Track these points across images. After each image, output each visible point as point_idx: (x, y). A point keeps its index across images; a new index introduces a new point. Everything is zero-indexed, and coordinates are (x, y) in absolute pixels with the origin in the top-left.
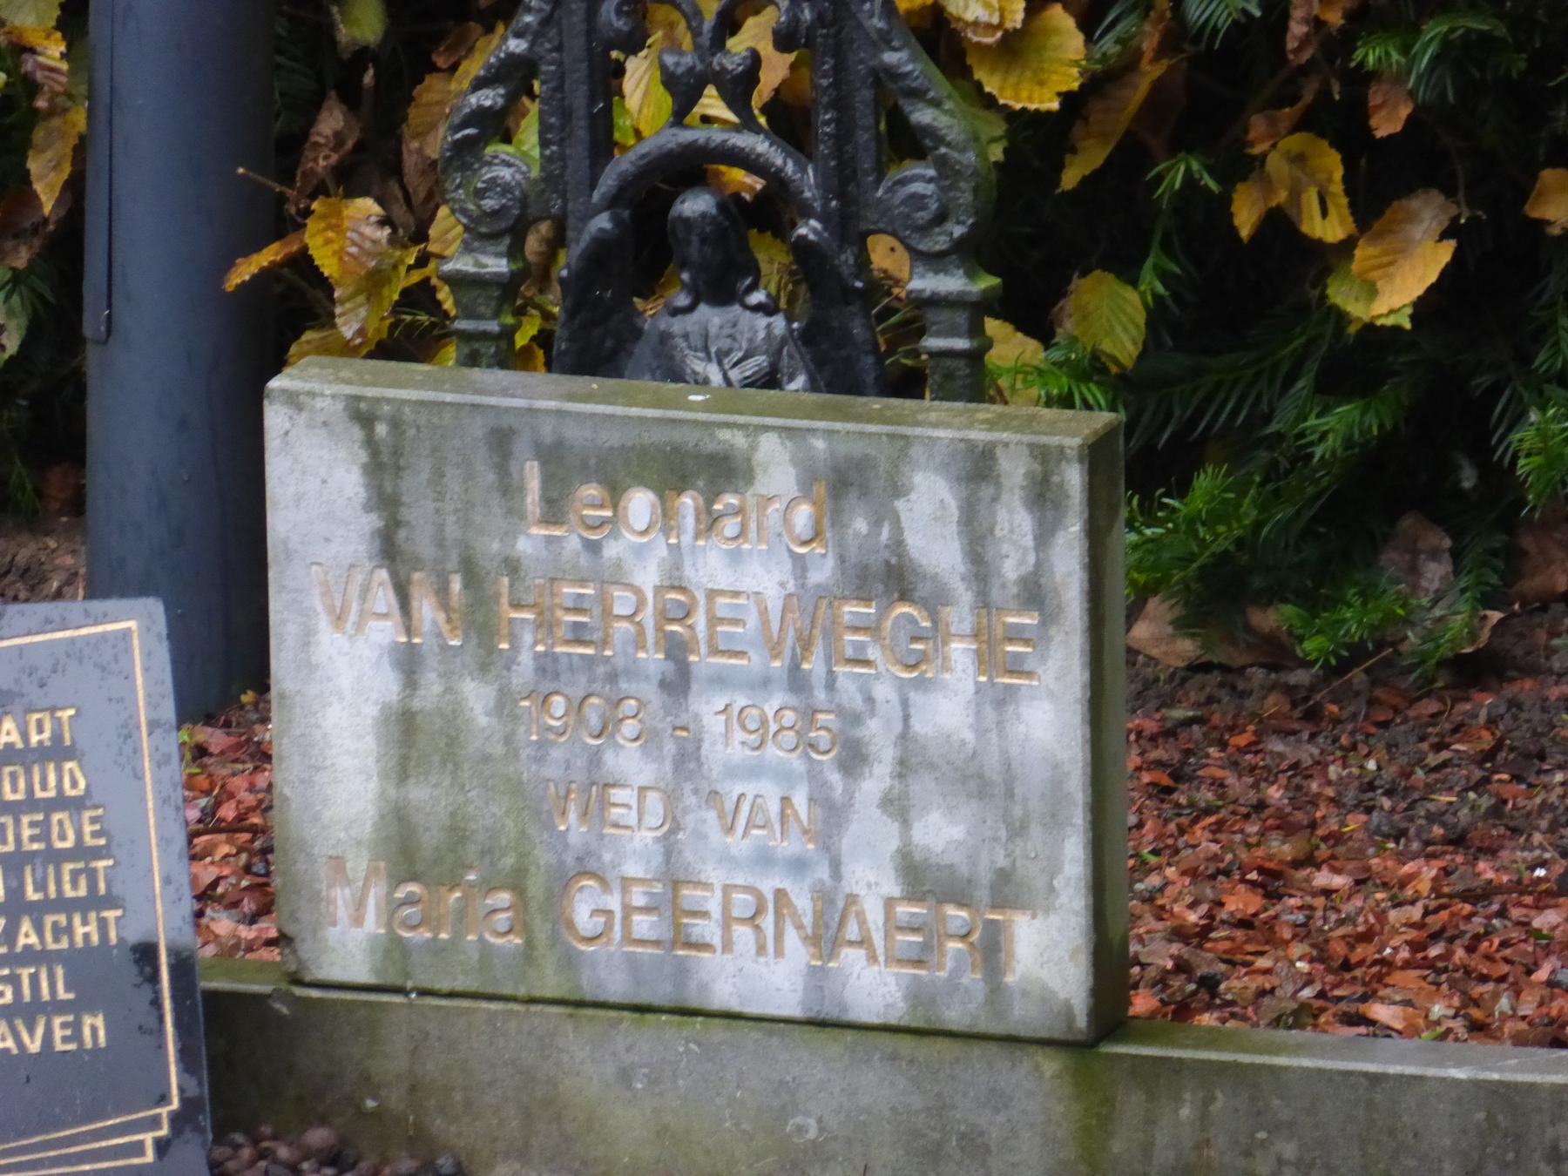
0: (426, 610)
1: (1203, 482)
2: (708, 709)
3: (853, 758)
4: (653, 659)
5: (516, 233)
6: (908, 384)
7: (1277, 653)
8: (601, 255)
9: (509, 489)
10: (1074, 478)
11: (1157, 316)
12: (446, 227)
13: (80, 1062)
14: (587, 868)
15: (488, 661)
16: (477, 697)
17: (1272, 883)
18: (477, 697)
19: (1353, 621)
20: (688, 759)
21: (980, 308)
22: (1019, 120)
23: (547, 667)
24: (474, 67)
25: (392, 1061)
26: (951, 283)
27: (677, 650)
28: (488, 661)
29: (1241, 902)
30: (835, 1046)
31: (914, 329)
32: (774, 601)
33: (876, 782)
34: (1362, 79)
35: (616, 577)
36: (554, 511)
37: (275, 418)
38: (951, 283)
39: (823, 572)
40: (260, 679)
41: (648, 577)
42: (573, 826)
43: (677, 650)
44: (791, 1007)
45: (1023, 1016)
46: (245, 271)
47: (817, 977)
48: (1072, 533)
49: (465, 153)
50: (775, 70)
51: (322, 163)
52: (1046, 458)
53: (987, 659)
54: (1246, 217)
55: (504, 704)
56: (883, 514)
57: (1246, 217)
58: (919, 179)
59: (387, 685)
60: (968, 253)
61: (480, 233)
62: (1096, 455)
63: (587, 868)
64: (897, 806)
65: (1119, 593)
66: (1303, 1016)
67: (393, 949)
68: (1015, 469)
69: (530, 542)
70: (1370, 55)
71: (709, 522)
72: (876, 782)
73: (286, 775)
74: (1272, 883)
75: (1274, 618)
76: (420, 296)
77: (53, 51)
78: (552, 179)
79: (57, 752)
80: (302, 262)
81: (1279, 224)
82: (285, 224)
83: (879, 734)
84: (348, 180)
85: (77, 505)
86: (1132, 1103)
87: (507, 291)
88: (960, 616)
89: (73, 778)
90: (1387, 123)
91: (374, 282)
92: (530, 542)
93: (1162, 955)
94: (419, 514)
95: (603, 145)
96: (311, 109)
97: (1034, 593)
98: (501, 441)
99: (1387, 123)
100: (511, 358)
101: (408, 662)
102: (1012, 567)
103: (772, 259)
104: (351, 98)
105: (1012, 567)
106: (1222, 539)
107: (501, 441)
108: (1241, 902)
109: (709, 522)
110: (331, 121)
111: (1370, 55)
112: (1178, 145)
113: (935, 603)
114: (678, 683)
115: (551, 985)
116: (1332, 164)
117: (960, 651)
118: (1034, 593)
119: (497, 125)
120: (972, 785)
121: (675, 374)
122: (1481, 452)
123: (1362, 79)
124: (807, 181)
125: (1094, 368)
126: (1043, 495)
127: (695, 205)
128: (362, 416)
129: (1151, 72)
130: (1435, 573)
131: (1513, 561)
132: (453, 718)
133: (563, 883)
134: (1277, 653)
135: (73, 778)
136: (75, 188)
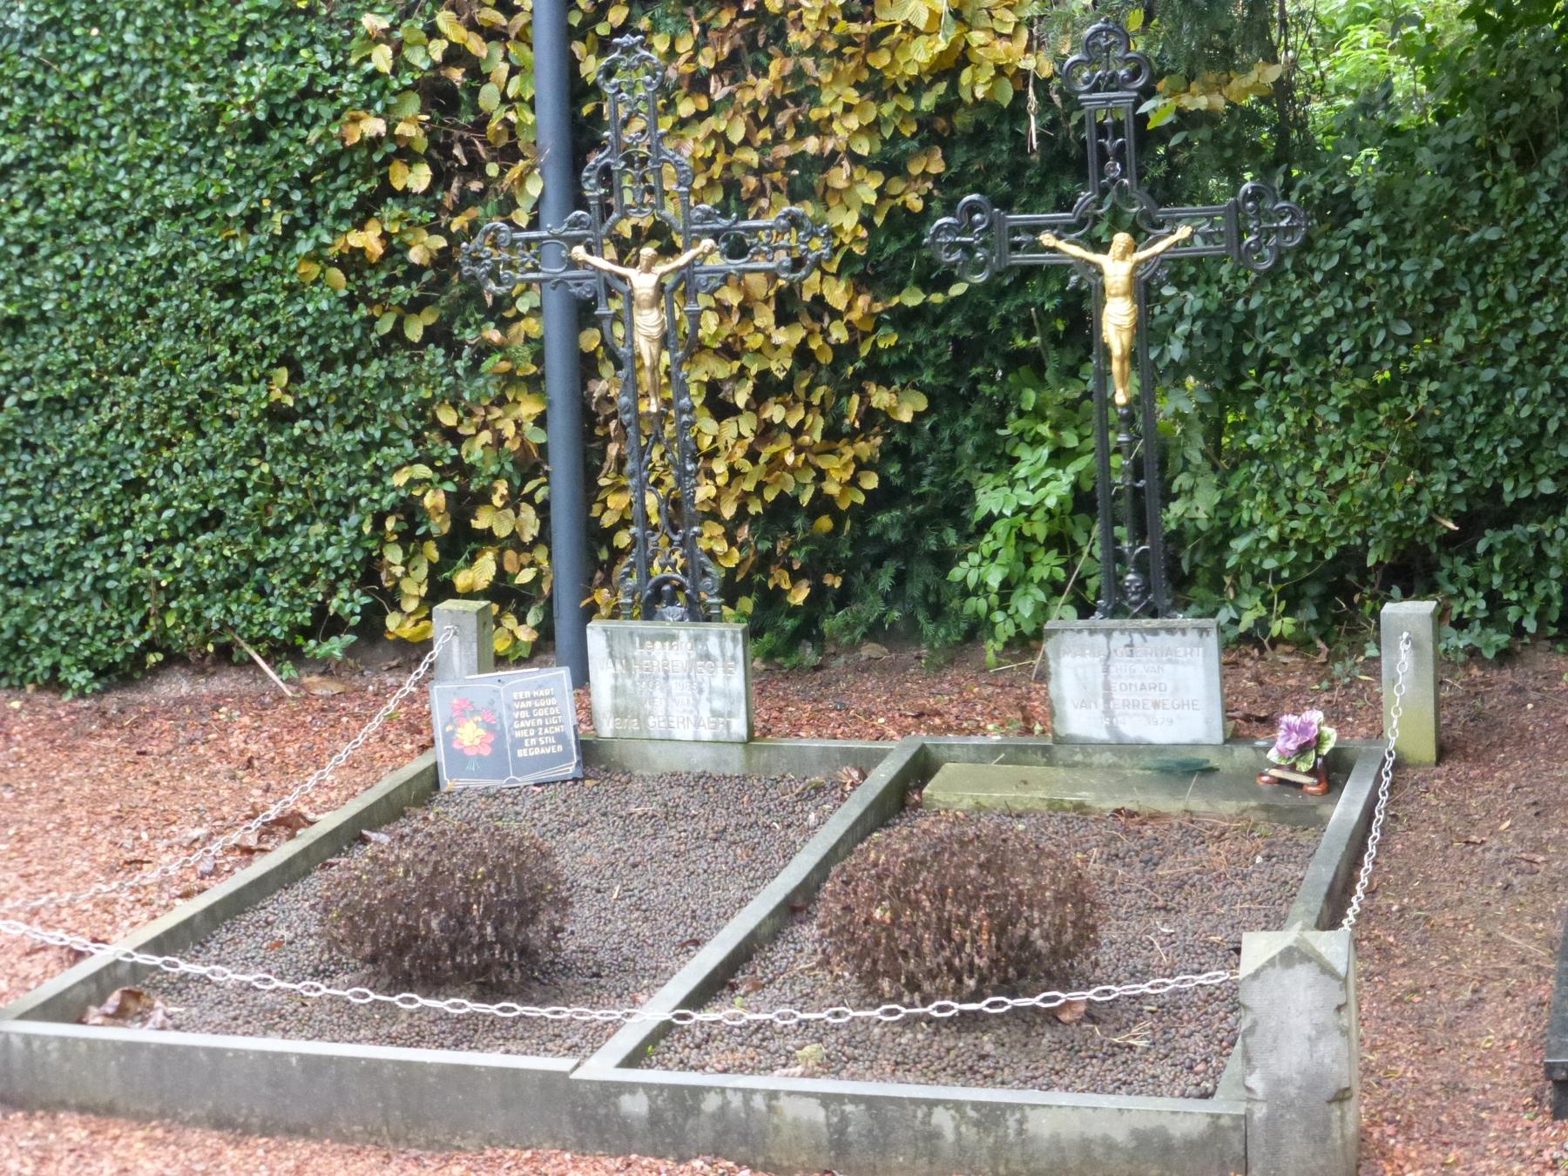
0: (618, 666)
1: (766, 636)
2: (672, 683)
3: (701, 691)
4: (662, 674)
5: (633, 595)
6: (708, 619)
7: (780, 667)
8: (649, 599)
9: (633, 643)
10: (740, 636)
11: (756, 605)
12: (620, 594)
13: (559, 754)
14: (651, 714)
15: (630, 675)
16: (629, 683)
17: (780, 710)
18: (629, 683)
19: (794, 660)
20: (669, 693)
21: (720, 605)
22: (728, 570)
23: (642, 676)
24: (625, 563)
25: (616, 752)
26: (715, 600)
27: (666, 672)
28: (630, 675)
29: (775, 714)
30: (699, 746)
31: (708, 609)
32: (752, 187)
33: (705, 695)
34: (791, 559)
35: (653, 659)
36: (642, 646)
37: (589, 632)
38: (715, 600)
39: (693, 655)
40: (587, 679)
41: (660, 658)
42: (648, 706)
43: (666, 672)
44: (690, 737)
45: (734, 738)
46: (583, 603)
47: (695, 733)
48: (740, 646)
49: (623, 580)
50: (681, 562)
51: (597, 582)
52: (735, 633)
53: (725, 671)
54: (771, 586)
55: (634, 684)
56: (705, 644)
57: (771, 586)
58: (708, 581)
59: (612, 681)
60: (719, 594)
61: (626, 594)
62: (744, 631)
63: (651, 714)
64: (709, 700)
65: (750, 654)
66: (787, 735)
67: (615, 730)
68: (729, 635)
69: (637, 652)
70: (792, 554)
71: (671, 647)
72: (705, 695)
73: (594, 698)
74: (780, 710)
75: (778, 660)
76: (616, 606)
77: (546, 564)
78: (639, 584)
79: (550, 696)
80: (594, 601)
81: (777, 586)
82: (590, 594)
83: (705, 686)
84: (602, 585)
85: (554, 648)
86: (756, 753)
87: (631, 605)
88: (720, 663)
89: (553, 701)
90: (796, 567)
91: (607, 604)
92: (637, 652)
93: (760, 725)
94: (616, 648)
95: (649, 577)
96: (594, 573)
97: (733, 658)
98: (631, 634)
99: (796, 567)
100: (632, 618)
101: (616, 677)
102: (729, 654)
103: (681, 597)
104: (602, 569)
105: (729, 654)
106: (768, 646)
107: (631, 634)
108: (775, 714)
109: (671, 647)
110: (599, 575)
111: (792, 554)
112: (758, 572)
113: (715, 661)
114: (667, 678)
115: (645, 735)
116: (787, 575)
117: (720, 670)
118: (733, 658)
119: (629, 575)
120: (799, 902)
121: (663, 619)
122: (816, 627)
123: (791, 559)
124: (687, 582)
125: (744, 614)
126: (734, 639)
127: (666, 588)
128: (605, 631)
129: (752, 559)
130: (809, 650)
131: (823, 648)
132: (624, 686)
133: (647, 717)
134: (780, 667)
135: (553, 701)
136: (551, 589)
